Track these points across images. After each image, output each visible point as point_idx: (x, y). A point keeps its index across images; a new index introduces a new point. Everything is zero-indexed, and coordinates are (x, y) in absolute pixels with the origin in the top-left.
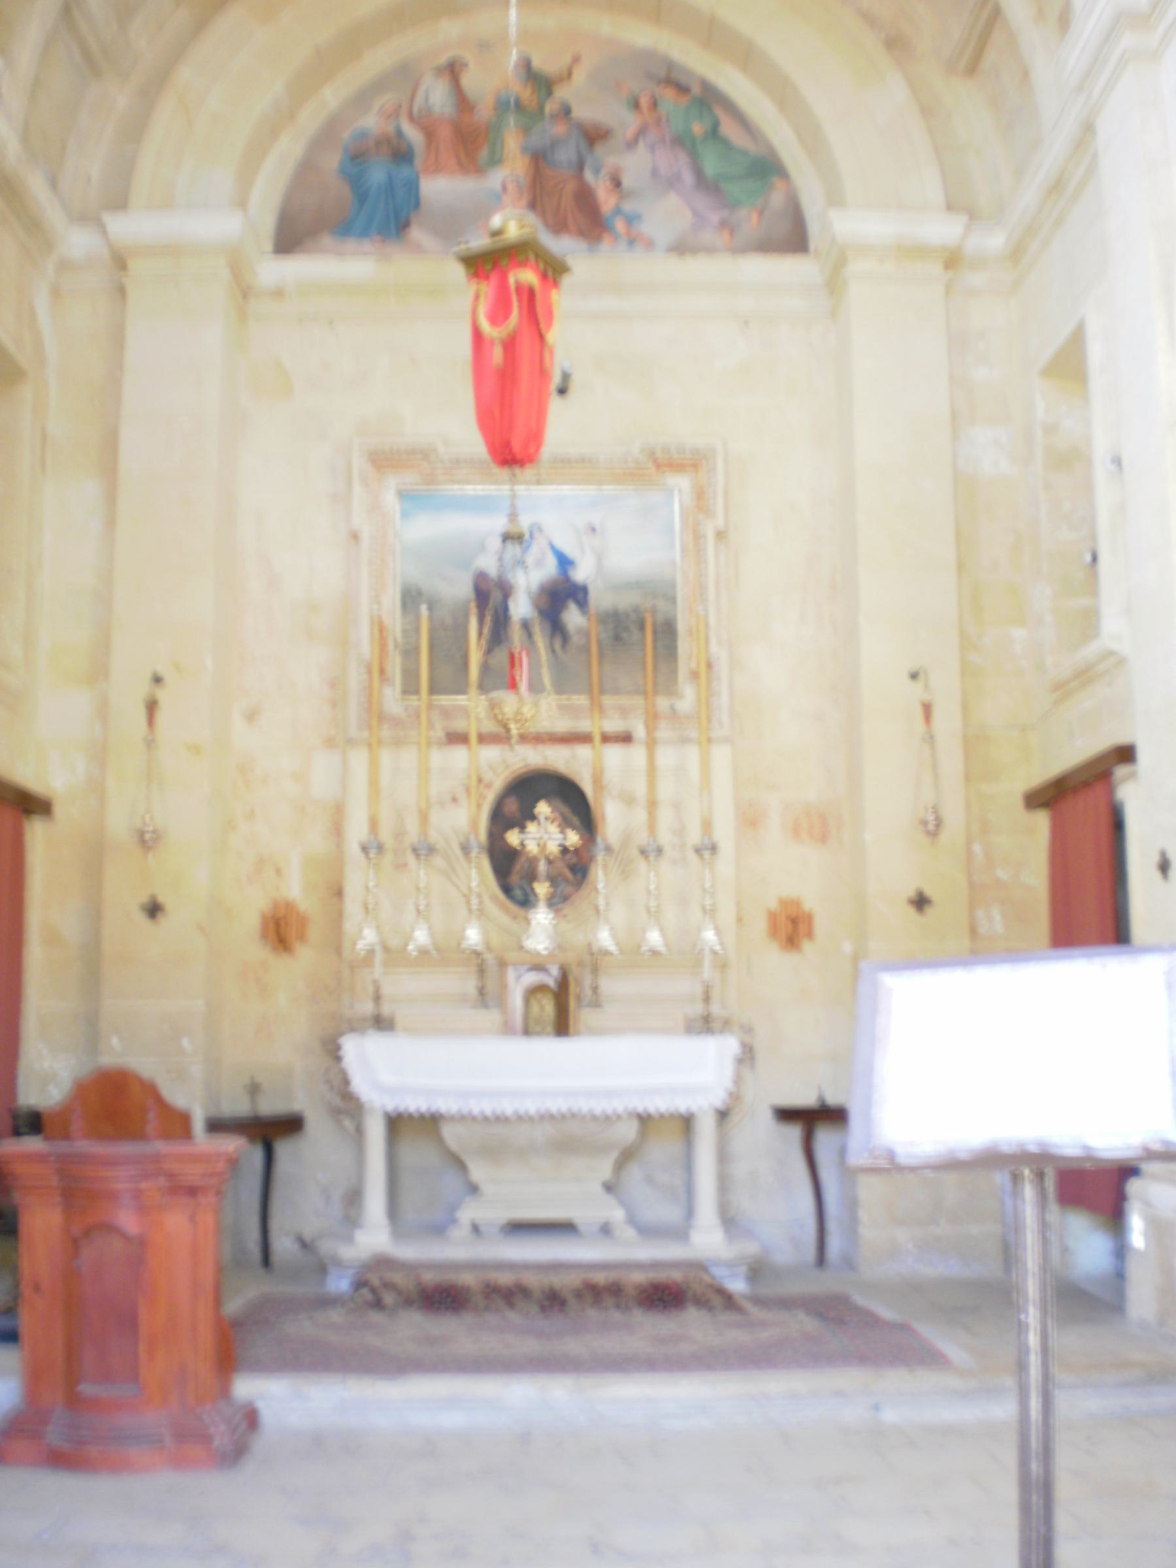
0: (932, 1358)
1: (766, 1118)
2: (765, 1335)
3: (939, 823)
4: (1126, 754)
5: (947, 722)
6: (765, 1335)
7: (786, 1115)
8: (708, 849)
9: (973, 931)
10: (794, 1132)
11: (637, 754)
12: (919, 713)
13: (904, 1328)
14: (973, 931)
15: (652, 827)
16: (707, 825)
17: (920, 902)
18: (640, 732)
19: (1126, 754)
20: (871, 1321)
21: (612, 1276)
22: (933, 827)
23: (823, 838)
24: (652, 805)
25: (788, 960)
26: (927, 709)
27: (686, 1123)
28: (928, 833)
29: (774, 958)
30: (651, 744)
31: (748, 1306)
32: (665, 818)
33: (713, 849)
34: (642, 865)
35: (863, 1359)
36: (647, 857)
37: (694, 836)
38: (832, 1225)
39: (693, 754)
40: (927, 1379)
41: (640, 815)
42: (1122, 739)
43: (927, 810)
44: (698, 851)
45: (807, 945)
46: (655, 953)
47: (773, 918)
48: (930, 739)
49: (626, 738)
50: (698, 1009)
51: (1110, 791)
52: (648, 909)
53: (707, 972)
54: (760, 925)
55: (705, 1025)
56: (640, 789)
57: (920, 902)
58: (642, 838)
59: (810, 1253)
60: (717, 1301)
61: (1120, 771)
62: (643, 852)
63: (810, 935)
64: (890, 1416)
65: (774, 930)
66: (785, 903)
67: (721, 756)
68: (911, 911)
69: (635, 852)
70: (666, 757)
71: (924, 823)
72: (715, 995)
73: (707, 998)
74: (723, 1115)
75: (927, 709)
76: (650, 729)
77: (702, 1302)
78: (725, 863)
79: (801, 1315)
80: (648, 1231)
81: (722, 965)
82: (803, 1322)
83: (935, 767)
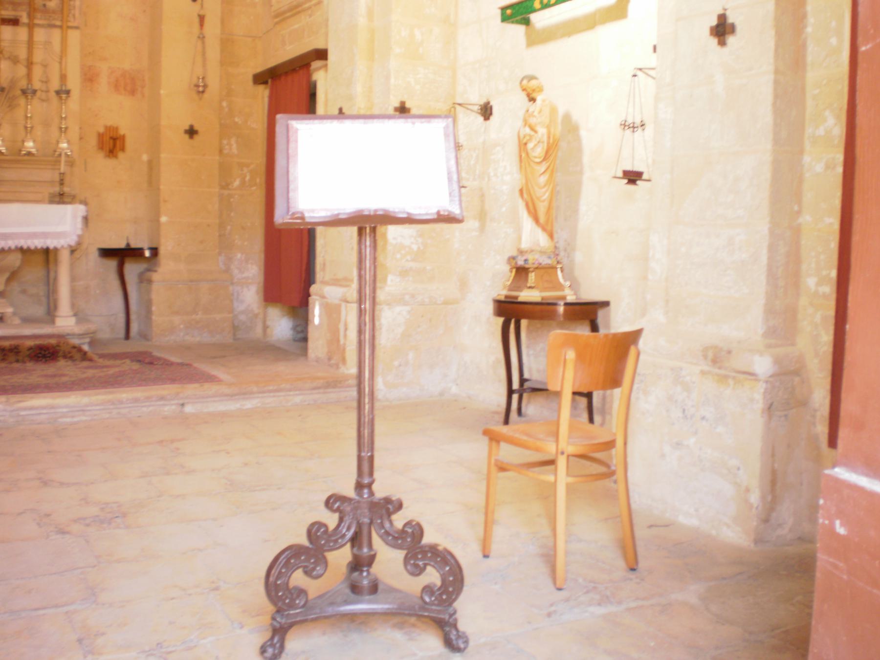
0: (211, 379)
1: (94, 255)
2: (112, 371)
3: (205, 86)
4: (321, 54)
5: (213, 29)
6: (112, 371)
7: (107, 253)
8: (63, 93)
9: (221, 151)
10: (112, 264)
11: (22, 33)
12: (197, 20)
13: (189, 365)
14: (221, 151)
15: (29, 76)
16: (63, 78)
17: (191, 132)
18: (25, 19)
19: (321, 54)
20: (168, 364)
21: (14, 342)
22: (200, 89)
23: (133, 92)
24: (30, 64)
25: (111, 162)
26: (202, 19)
27: (48, 255)
28: (199, 92)
29: (100, 162)
30: (31, 27)
31: (96, 358)
32: (37, 72)
33: (68, 92)
34: (22, 101)
35: (173, 381)
36: (26, 97)
37: (55, 84)
38: (133, 317)
39: (56, 34)
40: (210, 389)
41: (22, 71)
42: (320, 45)
43: (199, 78)
44: (58, 93)
45: (121, 155)
46: (29, 154)
47: (100, 136)
48: (202, 38)
49: (15, 22)
50: (57, 189)
51: (309, 75)
52: (26, 128)
53: (63, 168)
54: (93, 141)
55: (60, 198)
56: (23, 54)
57: (191, 132)
58: (23, 83)
59: (122, 333)
60: (77, 356)
61: (316, 64)
62: (24, 92)
63: (123, 149)
64: (188, 409)
65: (101, 146)
66: (108, 129)
67: (74, 36)
68: (187, 136)
69: (19, 92)
70: (40, 35)
71: (197, 86)
72: (66, 181)
73: (62, 182)
74: (73, 251)
75: (202, 19)
76: (30, 16)
77: (68, 356)
78: (74, 103)
79: (128, 361)
80: (28, 320)
81: (71, 163)
82: (128, 365)
83: (204, 54)
